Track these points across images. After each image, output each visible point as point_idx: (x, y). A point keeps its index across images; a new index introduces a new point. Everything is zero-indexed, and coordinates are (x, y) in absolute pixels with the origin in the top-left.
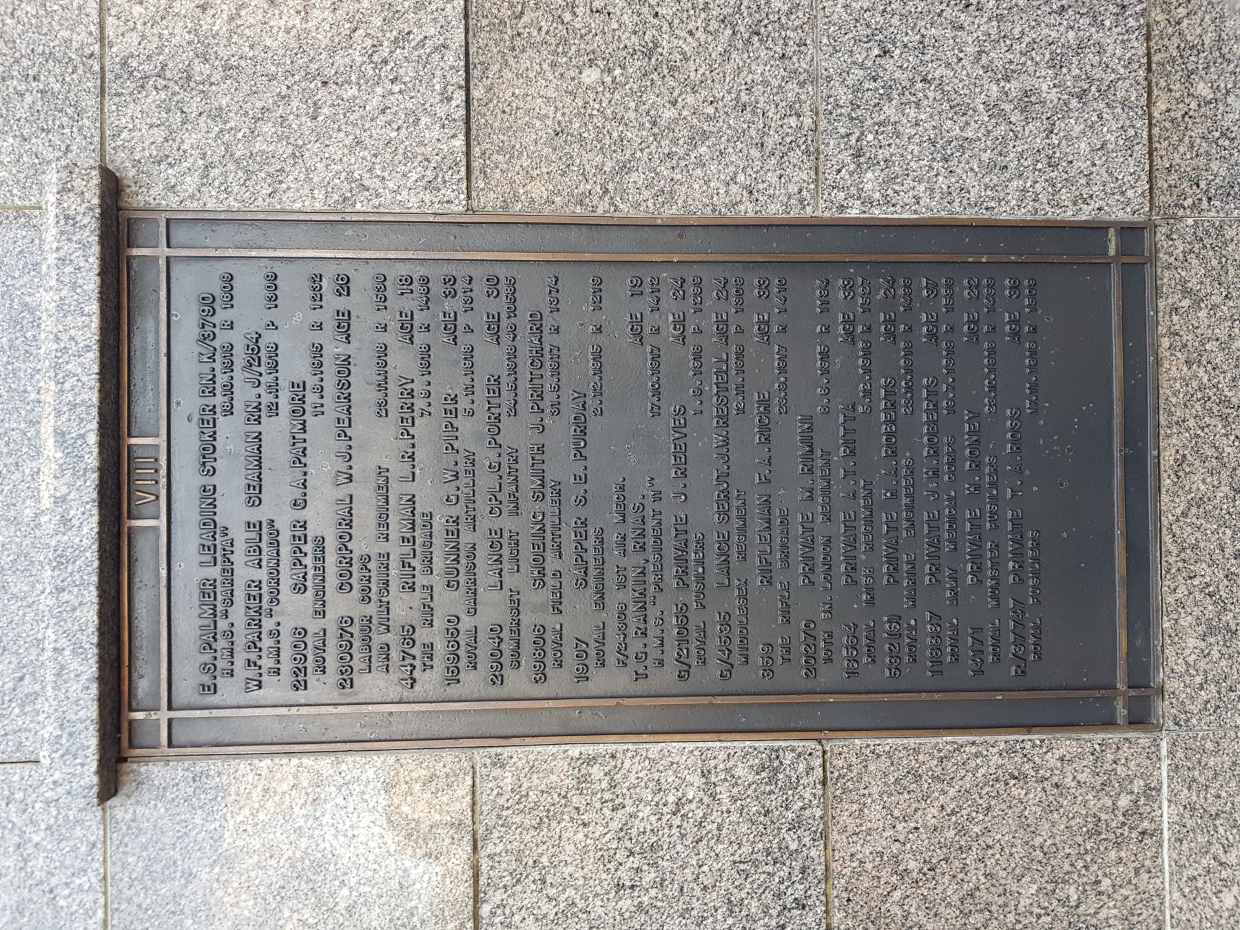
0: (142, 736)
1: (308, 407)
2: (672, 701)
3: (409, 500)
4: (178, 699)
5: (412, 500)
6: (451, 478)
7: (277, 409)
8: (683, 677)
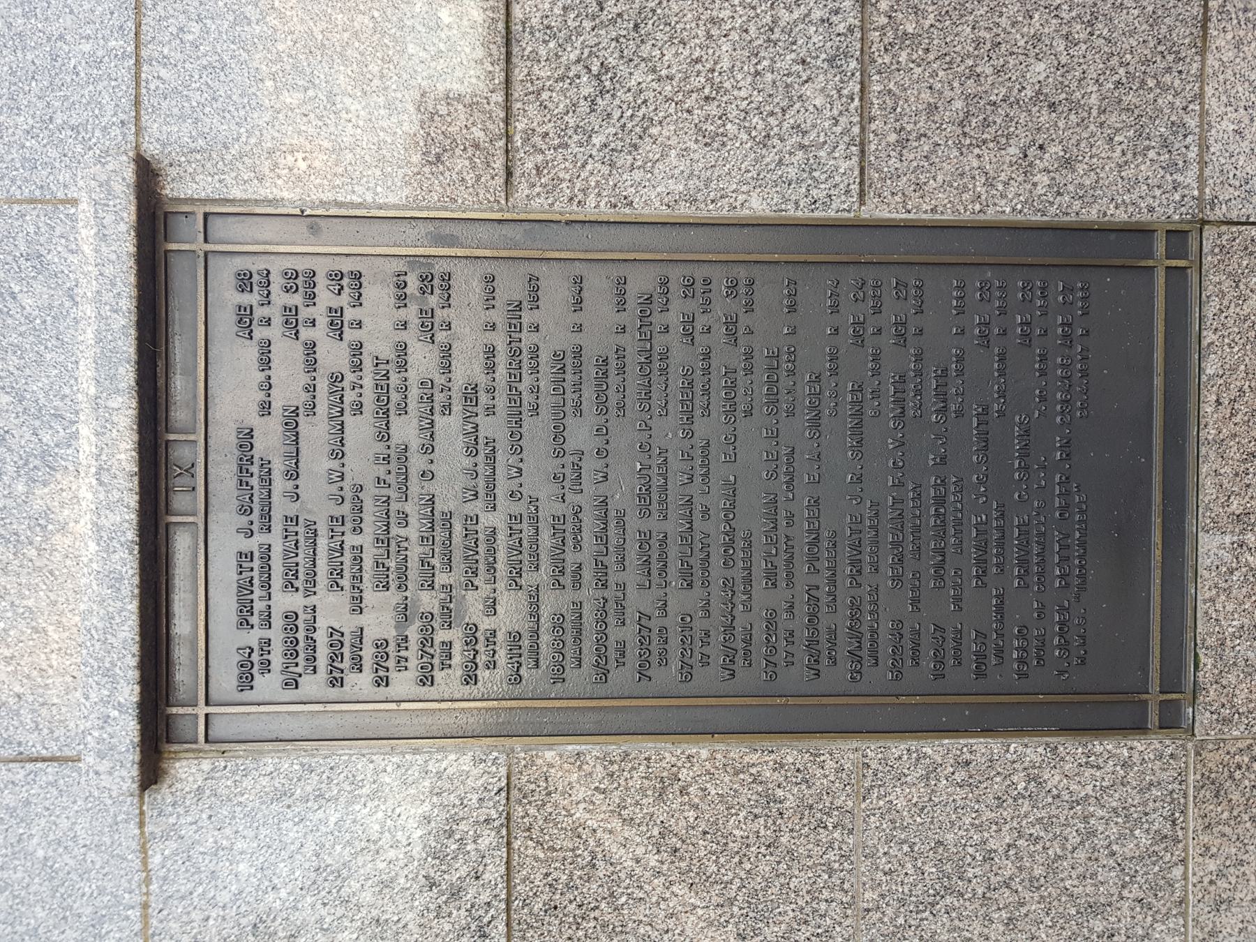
0: (182, 727)
1: (346, 406)
2: (749, 701)
3: (430, 500)
4: (214, 695)
5: (432, 500)
6: (601, 479)
7: (270, 408)
8: (855, 678)
